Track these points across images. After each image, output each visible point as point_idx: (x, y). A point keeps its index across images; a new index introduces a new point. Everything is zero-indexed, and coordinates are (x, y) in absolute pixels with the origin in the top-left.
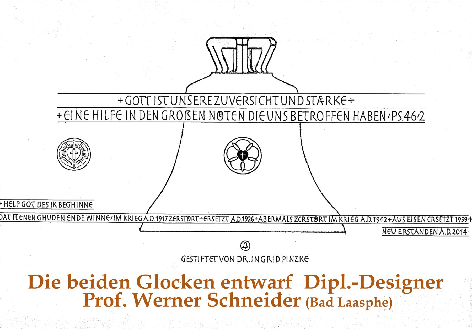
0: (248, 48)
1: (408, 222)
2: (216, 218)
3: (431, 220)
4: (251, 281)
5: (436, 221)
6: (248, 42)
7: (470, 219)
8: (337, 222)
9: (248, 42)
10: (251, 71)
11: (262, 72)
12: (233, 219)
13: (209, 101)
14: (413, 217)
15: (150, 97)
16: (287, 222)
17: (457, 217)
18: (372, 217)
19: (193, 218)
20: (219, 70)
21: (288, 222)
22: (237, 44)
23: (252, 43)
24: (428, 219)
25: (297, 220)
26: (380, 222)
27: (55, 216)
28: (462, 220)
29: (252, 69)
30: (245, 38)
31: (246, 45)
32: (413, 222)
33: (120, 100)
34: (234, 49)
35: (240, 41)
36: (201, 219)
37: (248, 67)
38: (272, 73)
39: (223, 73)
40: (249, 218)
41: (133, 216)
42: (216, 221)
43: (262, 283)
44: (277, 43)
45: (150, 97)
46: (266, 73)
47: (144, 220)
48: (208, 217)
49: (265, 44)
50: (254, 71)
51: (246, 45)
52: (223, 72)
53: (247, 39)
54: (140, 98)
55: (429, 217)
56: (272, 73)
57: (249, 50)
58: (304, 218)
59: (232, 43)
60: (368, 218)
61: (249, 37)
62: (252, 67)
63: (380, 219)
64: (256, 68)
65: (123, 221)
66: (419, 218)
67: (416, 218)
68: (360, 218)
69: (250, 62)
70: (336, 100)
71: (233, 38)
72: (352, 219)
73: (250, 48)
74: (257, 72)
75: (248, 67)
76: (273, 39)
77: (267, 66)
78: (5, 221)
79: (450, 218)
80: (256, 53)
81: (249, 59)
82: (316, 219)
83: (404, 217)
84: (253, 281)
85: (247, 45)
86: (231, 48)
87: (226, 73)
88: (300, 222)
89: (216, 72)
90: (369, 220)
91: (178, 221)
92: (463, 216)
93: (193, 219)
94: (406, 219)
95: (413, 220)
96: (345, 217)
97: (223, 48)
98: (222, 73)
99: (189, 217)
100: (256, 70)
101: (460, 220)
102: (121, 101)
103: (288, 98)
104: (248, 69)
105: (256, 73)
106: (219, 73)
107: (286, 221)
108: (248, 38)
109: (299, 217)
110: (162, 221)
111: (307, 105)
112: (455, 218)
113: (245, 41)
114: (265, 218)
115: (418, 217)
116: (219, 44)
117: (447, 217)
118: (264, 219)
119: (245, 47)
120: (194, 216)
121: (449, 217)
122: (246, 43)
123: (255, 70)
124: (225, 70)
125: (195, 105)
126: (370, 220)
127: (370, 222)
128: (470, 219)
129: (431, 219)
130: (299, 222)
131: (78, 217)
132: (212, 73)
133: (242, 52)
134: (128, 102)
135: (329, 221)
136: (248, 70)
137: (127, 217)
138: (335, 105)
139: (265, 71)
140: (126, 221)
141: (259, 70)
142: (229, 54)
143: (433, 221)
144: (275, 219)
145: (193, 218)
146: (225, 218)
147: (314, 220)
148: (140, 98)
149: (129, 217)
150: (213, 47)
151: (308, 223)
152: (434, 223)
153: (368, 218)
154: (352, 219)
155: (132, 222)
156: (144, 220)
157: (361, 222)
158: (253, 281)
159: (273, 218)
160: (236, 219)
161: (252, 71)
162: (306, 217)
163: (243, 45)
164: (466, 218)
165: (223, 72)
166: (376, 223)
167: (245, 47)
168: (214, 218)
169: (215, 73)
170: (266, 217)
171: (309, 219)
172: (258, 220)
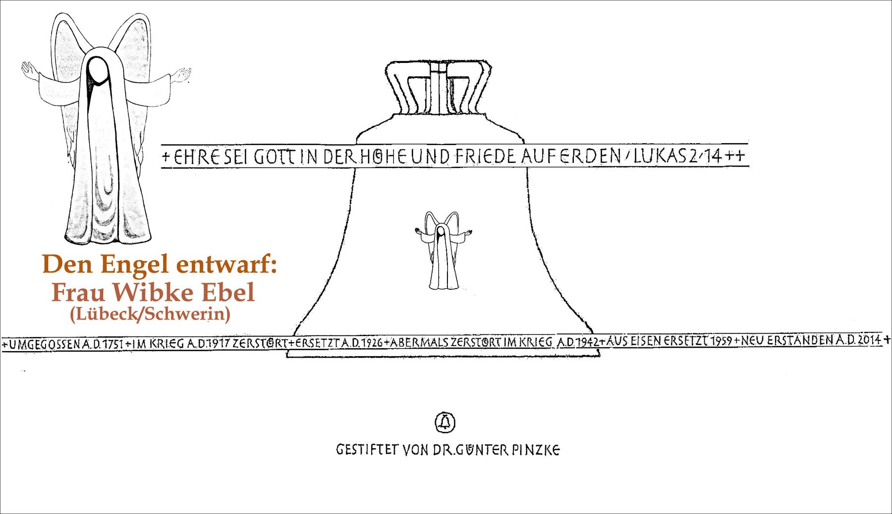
0: (447, 78)
1: (632, 344)
2: (36, 343)
3: (463, 342)
4: (215, 262)
5: (678, 344)
6: (447, 69)
7: (887, 339)
8: (515, 345)
9: (447, 69)
10: (454, 112)
11: (470, 113)
12: (86, 344)
13: (338, 157)
14: (641, 336)
15: (605, 149)
16: (438, 347)
17: (713, 338)
18: (101, 340)
19: (492, 340)
20: (405, 111)
21: (439, 346)
22: (431, 72)
23: (453, 69)
24: (665, 340)
25: (456, 343)
26: (588, 345)
27: (572, 339)
28: (723, 342)
29: (454, 109)
30: (443, 62)
31: (444, 72)
32: (640, 346)
33: (166, 156)
34: (426, 78)
35: (435, 67)
36: (291, 343)
37: (447, 105)
38: (485, 114)
39: (411, 114)
40: (373, 342)
41: (167, 340)
42: (69, 348)
43: (186, 315)
44: (492, 69)
45: (605, 149)
46: (475, 114)
47: (837, 342)
48: (528, 338)
49: (473, 71)
50: (457, 112)
51: (444, 72)
52: (410, 112)
53: (445, 63)
54: (278, 153)
55: (667, 336)
56: (485, 114)
57: (449, 80)
58: (467, 340)
59: (424, 69)
60: (199, 342)
61: (449, 60)
62: (454, 105)
63: (587, 342)
64: (461, 106)
65: (148, 348)
66: (650, 338)
67: (646, 339)
68: (186, 342)
69: (451, 99)
70: (659, 155)
71: (424, 61)
72: (667, 340)
73: (450, 78)
74: (461, 113)
75: (447, 105)
76: (486, 62)
77: (477, 103)
78: (220, 349)
79: (702, 339)
80: (460, 85)
81: (449, 94)
82: (270, 342)
83: (680, 336)
84: (218, 262)
85: (446, 72)
86: (421, 77)
87: (414, 114)
88: (668, 344)
89: (400, 114)
90: (355, 344)
91: (306, 347)
92: (725, 335)
93: (306, 343)
94: (629, 340)
95: (641, 342)
96: (778, 336)
97: (410, 78)
98: (408, 114)
99: (485, 338)
100: (460, 109)
101: (719, 342)
102: (731, 156)
103: (306, 154)
104: (448, 108)
105: (461, 114)
106: (405, 114)
107: (438, 345)
108: (447, 62)
109: (239, 339)
110: (219, 347)
111: (225, 163)
112: (362, 340)
113: (443, 67)
114: (401, 340)
115: (36, 341)
116: (403, 71)
117: (698, 336)
118: (400, 342)
119: (443, 76)
120: (494, 337)
121: (700, 337)
122: (445, 70)
123: (458, 110)
124: (413, 109)
125: (509, 162)
126: (357, 344)
127: (852, 343)
128: (887, 339)
129: (464, 341)
130: (458, 346)
131: (570, 340)
132: (394, 114)
133: (438, 83)
134: (259, 161)
135: (505, 346)
136: (448, 111)
137: (526, 340)
138: (346, 163)
139: (474, 111)
140: (153, 348)
141: (465, 110)
142: (418, 86)
143: (305, 344)
144: (419, 342)
145: (492, 340)
146: (334, 341)
147: (483, 344)
148: (278, 153)
149: (160, 342)
150: (395, 76)
151: (312, 348)
152: (676, 346)
153: (199, 342)
154: (667, 340)
155: (157, 349)
156: (837, 342)
157: (188, 347)
158: (218, 262)
159: (415, 340)
160: (565, 341)
161: (454, 111)
162: (254, 339)
163: (439, 72)
164: (729, 339)
165: (410, 112)
166: (366, 347)
167: (443, 76)
168: (314, 342)
169: (399, 114)
170: (402, 339)
171: (260, 342)
172: (389, 344)
